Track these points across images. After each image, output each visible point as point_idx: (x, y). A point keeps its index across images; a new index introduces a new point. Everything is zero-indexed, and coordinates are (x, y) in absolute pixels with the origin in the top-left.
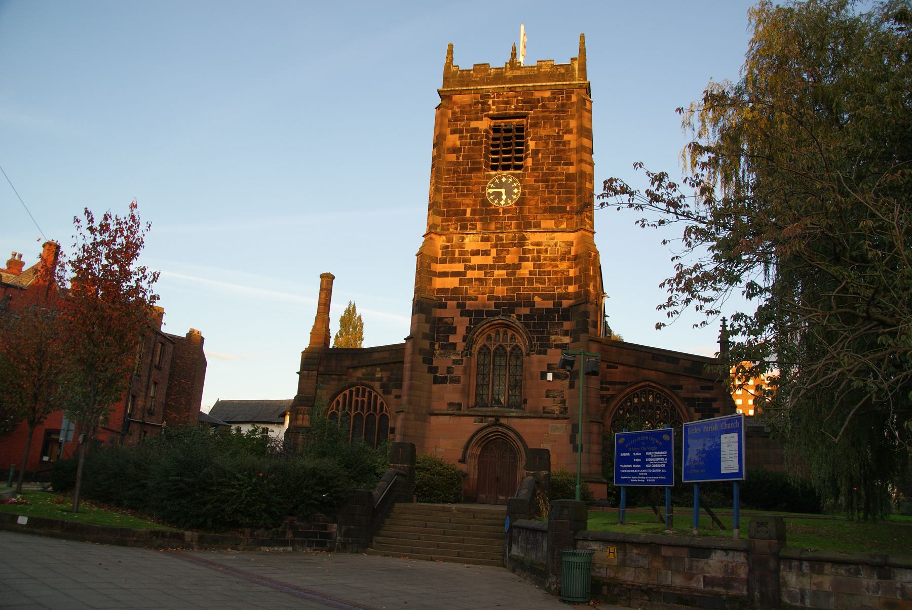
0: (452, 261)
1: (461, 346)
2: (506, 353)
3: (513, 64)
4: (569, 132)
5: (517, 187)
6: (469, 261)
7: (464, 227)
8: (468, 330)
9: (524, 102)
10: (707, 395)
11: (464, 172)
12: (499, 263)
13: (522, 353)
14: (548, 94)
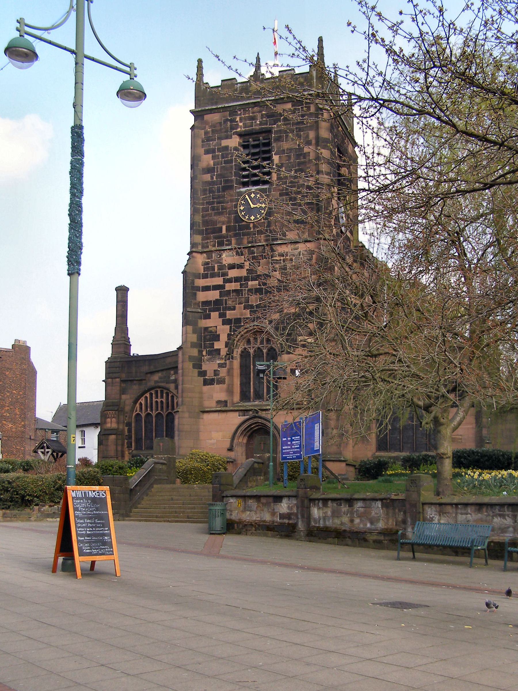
0: (213, 276)
1: (224, 352)
3: (257, 76)
6: (226, 274)
7: (221, 244)
8: (229, 335)
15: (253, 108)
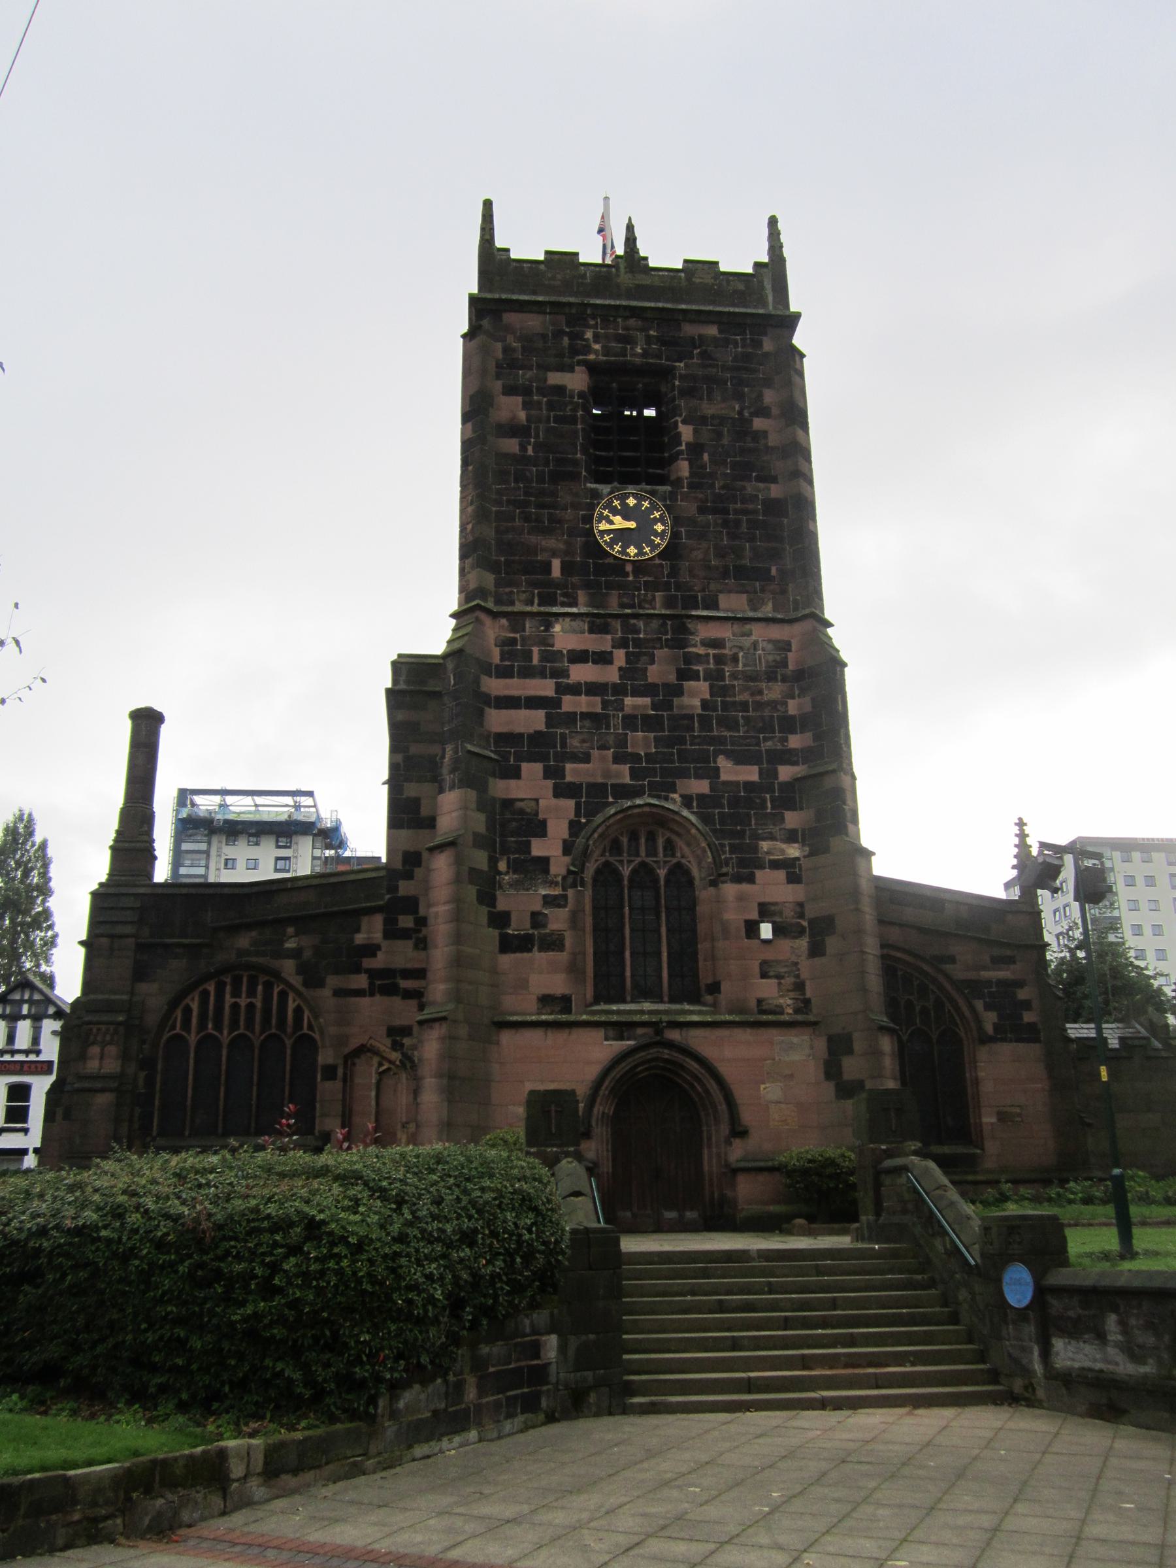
0: (528, 672)
1: (559, 866)
2: (656, 880)
4: (763, 412)
5: (661, 520)
6: (565, 673)
7: (548, 599)
8: (575, 827)
9: (661, 340)
10: (1003, 974)
11: (541, 479)
13: (691, 882)
15: (626, 318)
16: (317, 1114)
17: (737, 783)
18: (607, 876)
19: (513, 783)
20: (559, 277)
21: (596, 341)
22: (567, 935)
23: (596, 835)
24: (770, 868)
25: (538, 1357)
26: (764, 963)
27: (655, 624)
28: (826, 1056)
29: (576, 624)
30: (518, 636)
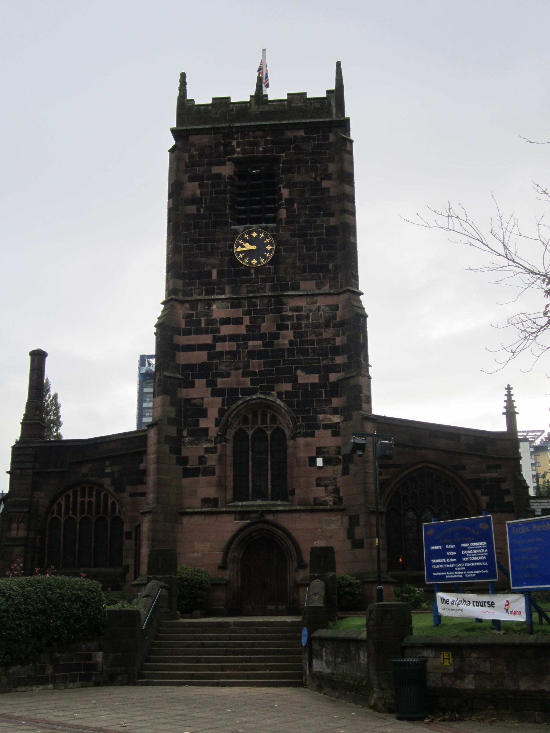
0: (199, 331)
1: (213, 432)
3: (259, 97)
4: (328, 177)
5: (270, 243)
7: (210, 292)
8: (221, 412)
10: (494, 475)
12: (253, 331)
13: (285, 436)
14: (301, 133)
16: (124, 556)
17: (307, 385)
18: (240, 435)
19: (190, 390)
20: (219, 112)
21: (238, 146)
22: (217, 467)
23: (232, 415)
24: (323, 429)
25: (90, 660)
26: (318, 479)
27: (266, 301)
28: (348, 526)
29: (225, 304)
30: (194, 312)
